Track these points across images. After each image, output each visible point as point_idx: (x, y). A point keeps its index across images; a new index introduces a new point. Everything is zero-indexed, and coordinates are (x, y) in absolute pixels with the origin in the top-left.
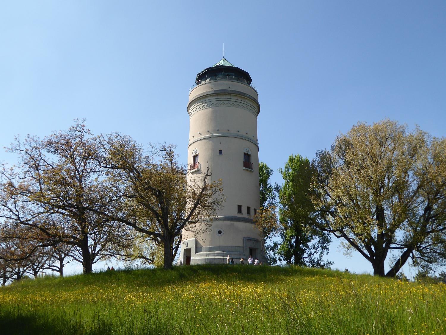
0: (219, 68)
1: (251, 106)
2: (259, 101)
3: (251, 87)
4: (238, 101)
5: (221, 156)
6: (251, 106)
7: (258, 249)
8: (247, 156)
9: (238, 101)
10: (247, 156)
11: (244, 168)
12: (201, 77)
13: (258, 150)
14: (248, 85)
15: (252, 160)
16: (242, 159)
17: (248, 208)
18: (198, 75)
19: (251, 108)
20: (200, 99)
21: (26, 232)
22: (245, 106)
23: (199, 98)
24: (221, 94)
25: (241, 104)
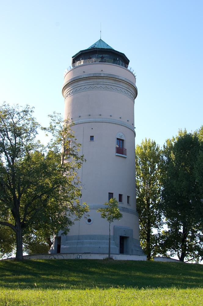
0: (93, 50)
1: (126, 88)
2: (137, 85)
3: (129, 71)
4: (111, 84)
5: (92, 142)
6: (126, 88)
7: (129, 237)
8: (120, 141)
9: (111, 84)
10: (120, 141)
11: (117, 154)
12: (76, 58)
13: (134, 134)
14: (125, 68)
15: (127, 146)
16: (114, 145)
17: (120, 196)
18: (73, 57)
19: (126, 91)
20: (77, 81)
21: (185, 168)
22: (119, 89)
23: (72, 83)
24: (83, 80)
25: (114, 88)
